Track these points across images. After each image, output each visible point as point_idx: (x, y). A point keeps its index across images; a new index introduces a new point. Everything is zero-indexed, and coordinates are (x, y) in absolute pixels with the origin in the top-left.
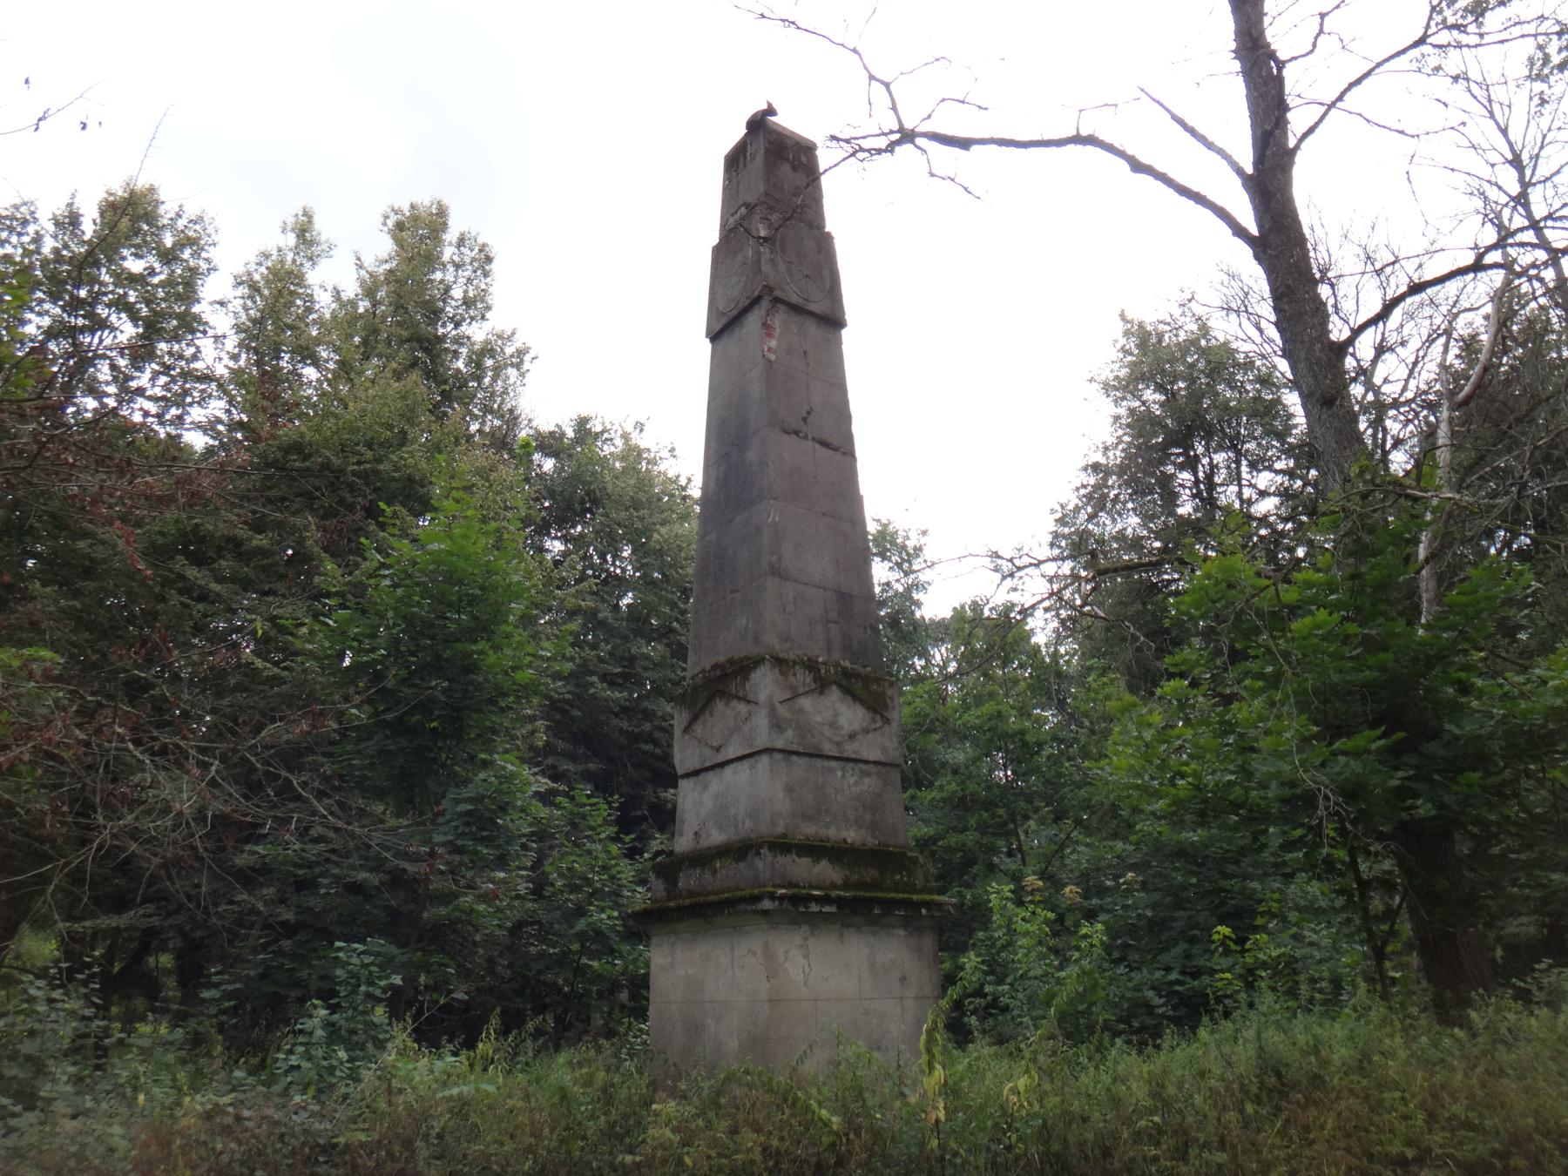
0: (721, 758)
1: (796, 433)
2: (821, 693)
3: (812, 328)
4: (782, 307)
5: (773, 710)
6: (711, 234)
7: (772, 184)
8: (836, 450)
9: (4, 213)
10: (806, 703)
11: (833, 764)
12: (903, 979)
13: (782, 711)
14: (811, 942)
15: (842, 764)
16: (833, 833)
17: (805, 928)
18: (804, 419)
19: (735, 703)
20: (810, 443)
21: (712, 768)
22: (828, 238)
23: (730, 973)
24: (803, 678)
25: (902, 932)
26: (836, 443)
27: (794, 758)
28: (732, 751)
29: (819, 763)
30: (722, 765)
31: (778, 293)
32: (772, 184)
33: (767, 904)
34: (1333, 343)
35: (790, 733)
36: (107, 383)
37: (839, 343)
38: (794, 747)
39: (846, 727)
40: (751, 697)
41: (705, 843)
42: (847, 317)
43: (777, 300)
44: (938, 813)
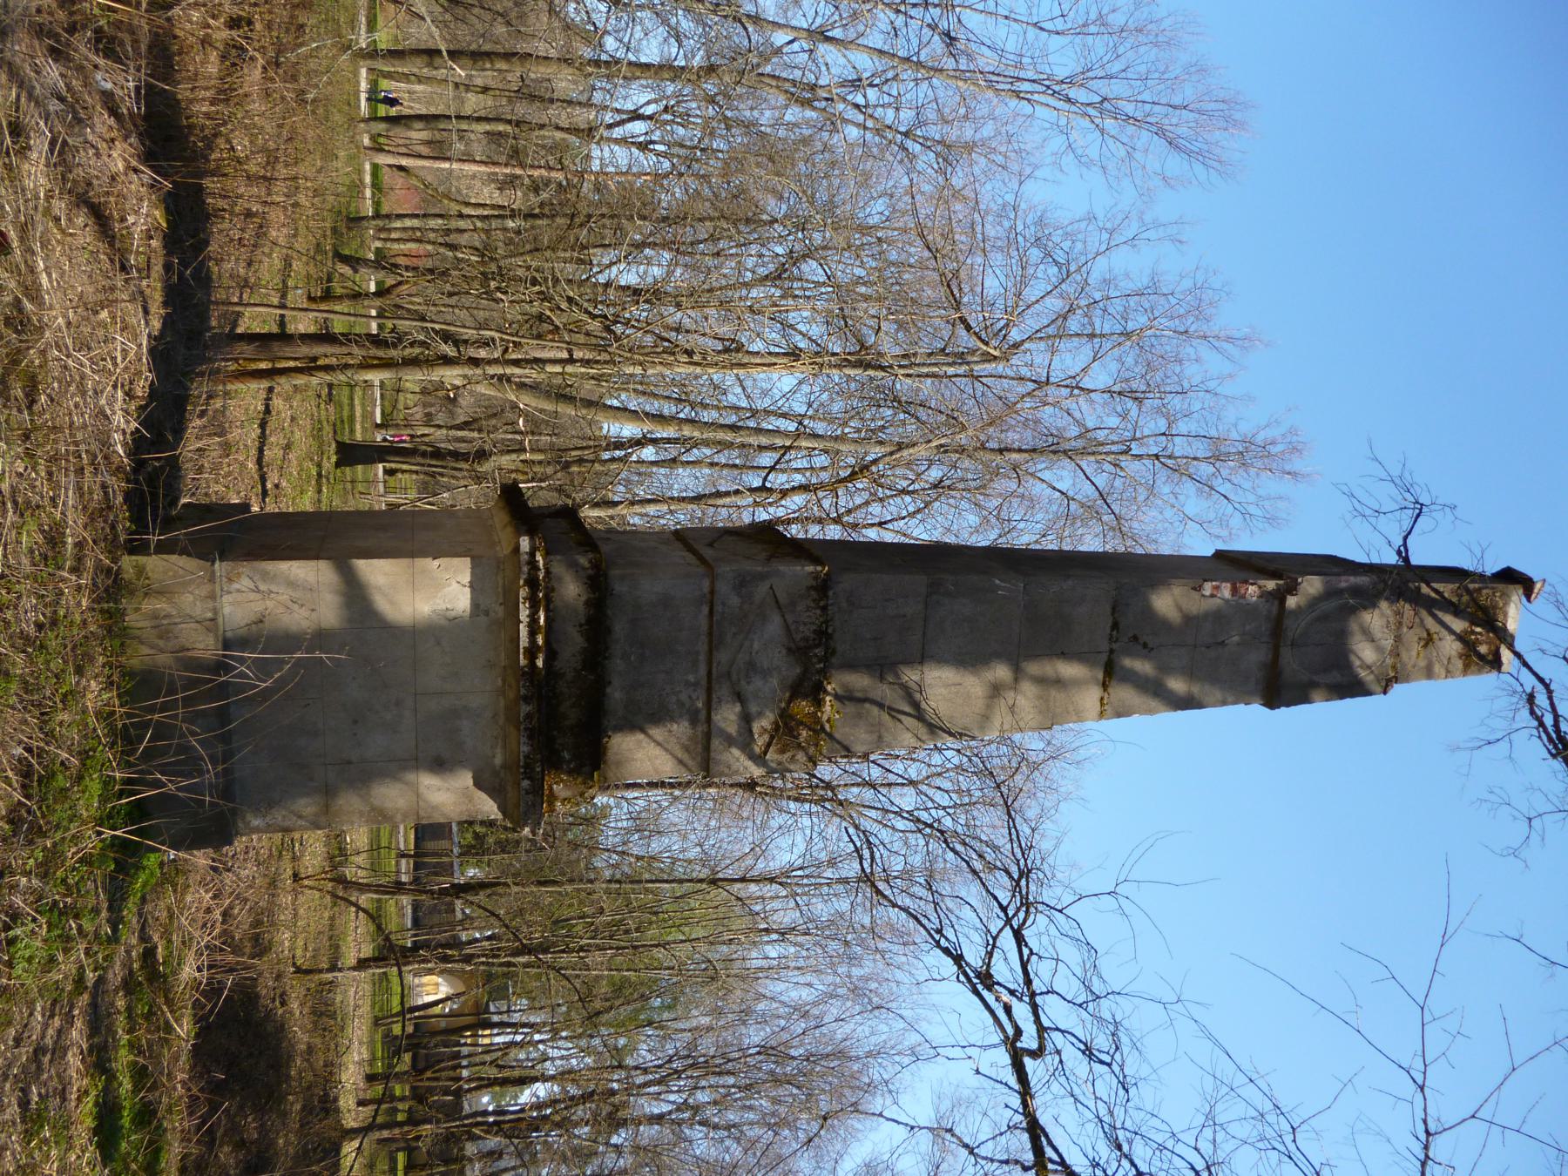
1: (1115, 626)
2: (789, 649)
3: (1257, 656)
5: (763, 577)
7: (1468, 609)
9: (344, 149)
10: (774, 626)
11: (703, 671)
13: (762, 590)
15: (704, 682)
16: (617, 666)
24: (807, 620)
27: (706, 610)
29: (702, 647)
34: (475, 604)
35: (735, 601)
37: (1242, 697)
38: (718, 608)
39: (751, 688)
42: (1283, 711)
44: (839, 1037)
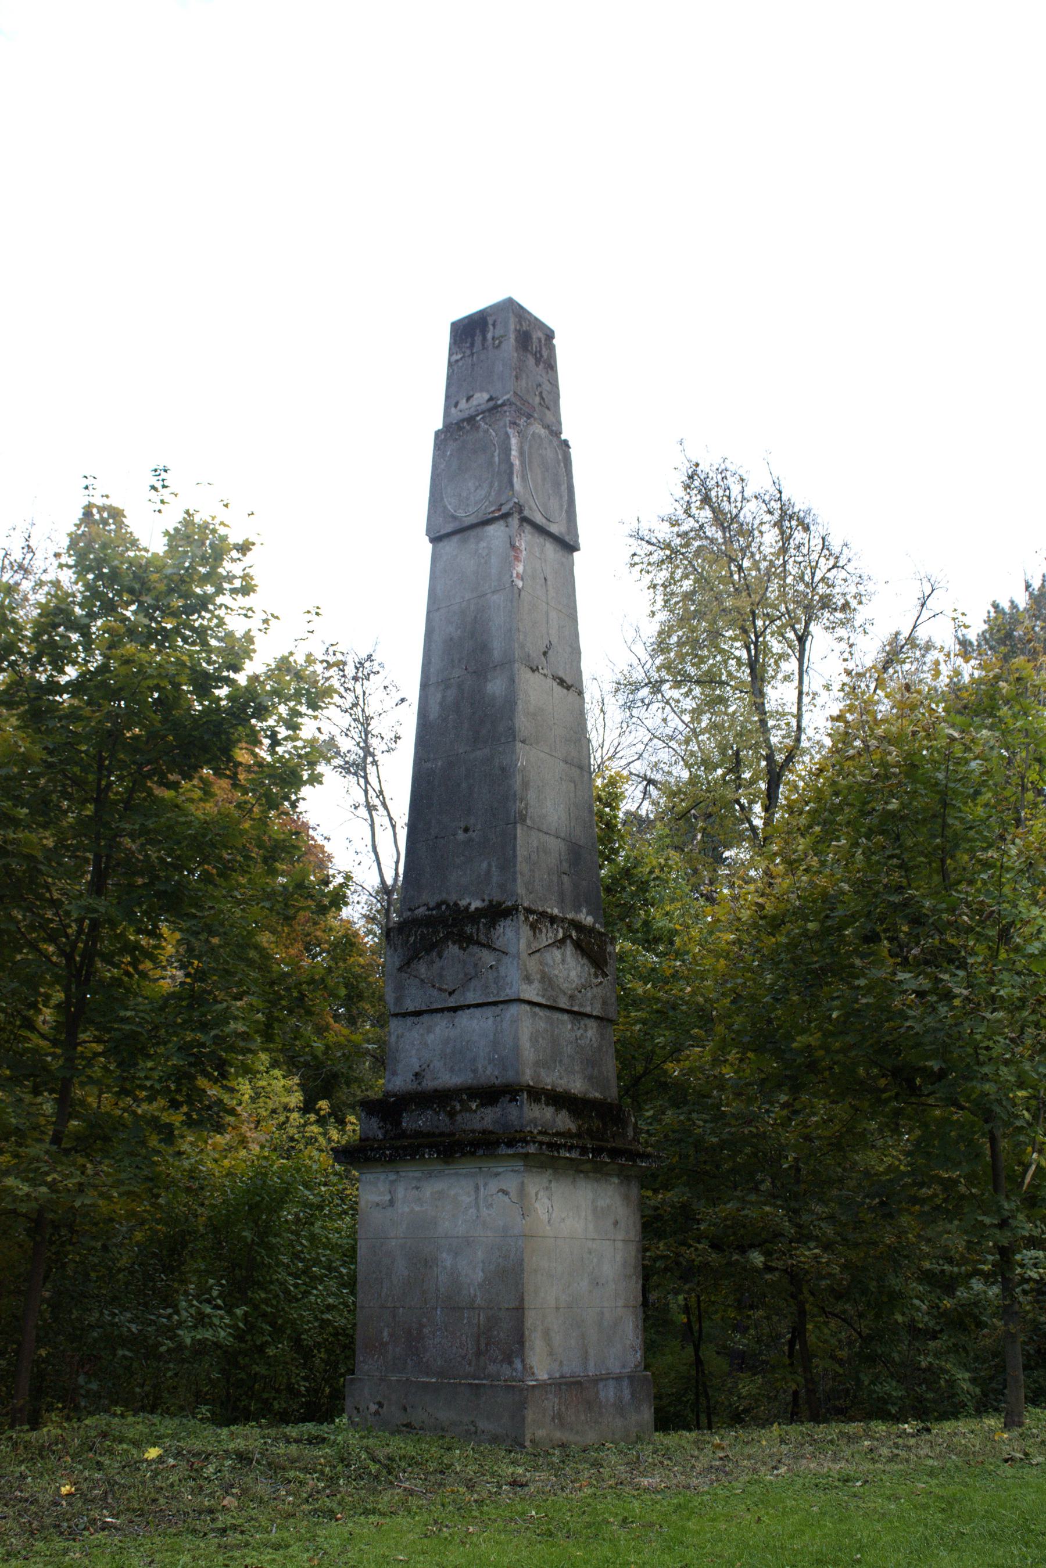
0: (451, 1002)
4: (528, 528)
6: (433, 417)
8: (568, 688)
12: (616, 1223)
14: (553, 1185)
17: (550, 1171)
18: (545, 654)
19: (474, 949)
20: (550, 681)
21: (441, 1010)
22: (566, 444)
23: (472, 1211)
25: (616, 1180)
26: (569, 681)
28: (471, 998)
30: (454, 1010)
31: (526, 513)
32: (501, 364)
33: (532, 1149)
36: (189, 692)
40: (498, 944)
41: (429, 1084)
43: (524, 520)
